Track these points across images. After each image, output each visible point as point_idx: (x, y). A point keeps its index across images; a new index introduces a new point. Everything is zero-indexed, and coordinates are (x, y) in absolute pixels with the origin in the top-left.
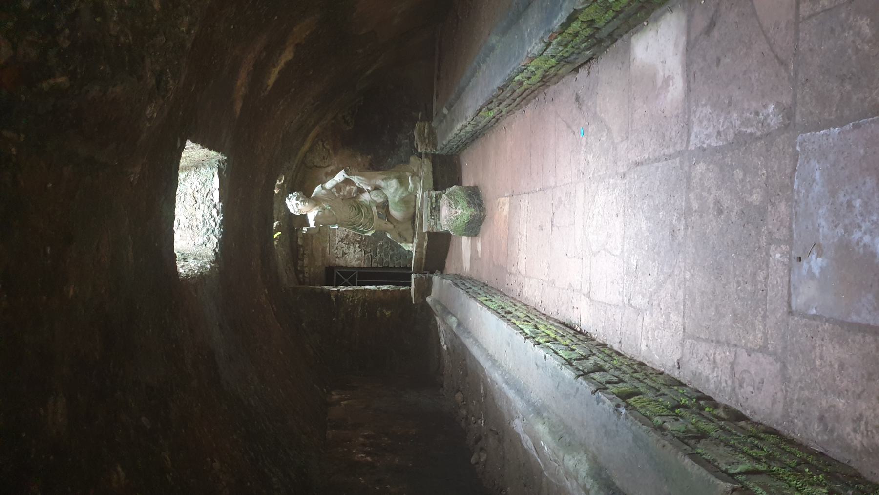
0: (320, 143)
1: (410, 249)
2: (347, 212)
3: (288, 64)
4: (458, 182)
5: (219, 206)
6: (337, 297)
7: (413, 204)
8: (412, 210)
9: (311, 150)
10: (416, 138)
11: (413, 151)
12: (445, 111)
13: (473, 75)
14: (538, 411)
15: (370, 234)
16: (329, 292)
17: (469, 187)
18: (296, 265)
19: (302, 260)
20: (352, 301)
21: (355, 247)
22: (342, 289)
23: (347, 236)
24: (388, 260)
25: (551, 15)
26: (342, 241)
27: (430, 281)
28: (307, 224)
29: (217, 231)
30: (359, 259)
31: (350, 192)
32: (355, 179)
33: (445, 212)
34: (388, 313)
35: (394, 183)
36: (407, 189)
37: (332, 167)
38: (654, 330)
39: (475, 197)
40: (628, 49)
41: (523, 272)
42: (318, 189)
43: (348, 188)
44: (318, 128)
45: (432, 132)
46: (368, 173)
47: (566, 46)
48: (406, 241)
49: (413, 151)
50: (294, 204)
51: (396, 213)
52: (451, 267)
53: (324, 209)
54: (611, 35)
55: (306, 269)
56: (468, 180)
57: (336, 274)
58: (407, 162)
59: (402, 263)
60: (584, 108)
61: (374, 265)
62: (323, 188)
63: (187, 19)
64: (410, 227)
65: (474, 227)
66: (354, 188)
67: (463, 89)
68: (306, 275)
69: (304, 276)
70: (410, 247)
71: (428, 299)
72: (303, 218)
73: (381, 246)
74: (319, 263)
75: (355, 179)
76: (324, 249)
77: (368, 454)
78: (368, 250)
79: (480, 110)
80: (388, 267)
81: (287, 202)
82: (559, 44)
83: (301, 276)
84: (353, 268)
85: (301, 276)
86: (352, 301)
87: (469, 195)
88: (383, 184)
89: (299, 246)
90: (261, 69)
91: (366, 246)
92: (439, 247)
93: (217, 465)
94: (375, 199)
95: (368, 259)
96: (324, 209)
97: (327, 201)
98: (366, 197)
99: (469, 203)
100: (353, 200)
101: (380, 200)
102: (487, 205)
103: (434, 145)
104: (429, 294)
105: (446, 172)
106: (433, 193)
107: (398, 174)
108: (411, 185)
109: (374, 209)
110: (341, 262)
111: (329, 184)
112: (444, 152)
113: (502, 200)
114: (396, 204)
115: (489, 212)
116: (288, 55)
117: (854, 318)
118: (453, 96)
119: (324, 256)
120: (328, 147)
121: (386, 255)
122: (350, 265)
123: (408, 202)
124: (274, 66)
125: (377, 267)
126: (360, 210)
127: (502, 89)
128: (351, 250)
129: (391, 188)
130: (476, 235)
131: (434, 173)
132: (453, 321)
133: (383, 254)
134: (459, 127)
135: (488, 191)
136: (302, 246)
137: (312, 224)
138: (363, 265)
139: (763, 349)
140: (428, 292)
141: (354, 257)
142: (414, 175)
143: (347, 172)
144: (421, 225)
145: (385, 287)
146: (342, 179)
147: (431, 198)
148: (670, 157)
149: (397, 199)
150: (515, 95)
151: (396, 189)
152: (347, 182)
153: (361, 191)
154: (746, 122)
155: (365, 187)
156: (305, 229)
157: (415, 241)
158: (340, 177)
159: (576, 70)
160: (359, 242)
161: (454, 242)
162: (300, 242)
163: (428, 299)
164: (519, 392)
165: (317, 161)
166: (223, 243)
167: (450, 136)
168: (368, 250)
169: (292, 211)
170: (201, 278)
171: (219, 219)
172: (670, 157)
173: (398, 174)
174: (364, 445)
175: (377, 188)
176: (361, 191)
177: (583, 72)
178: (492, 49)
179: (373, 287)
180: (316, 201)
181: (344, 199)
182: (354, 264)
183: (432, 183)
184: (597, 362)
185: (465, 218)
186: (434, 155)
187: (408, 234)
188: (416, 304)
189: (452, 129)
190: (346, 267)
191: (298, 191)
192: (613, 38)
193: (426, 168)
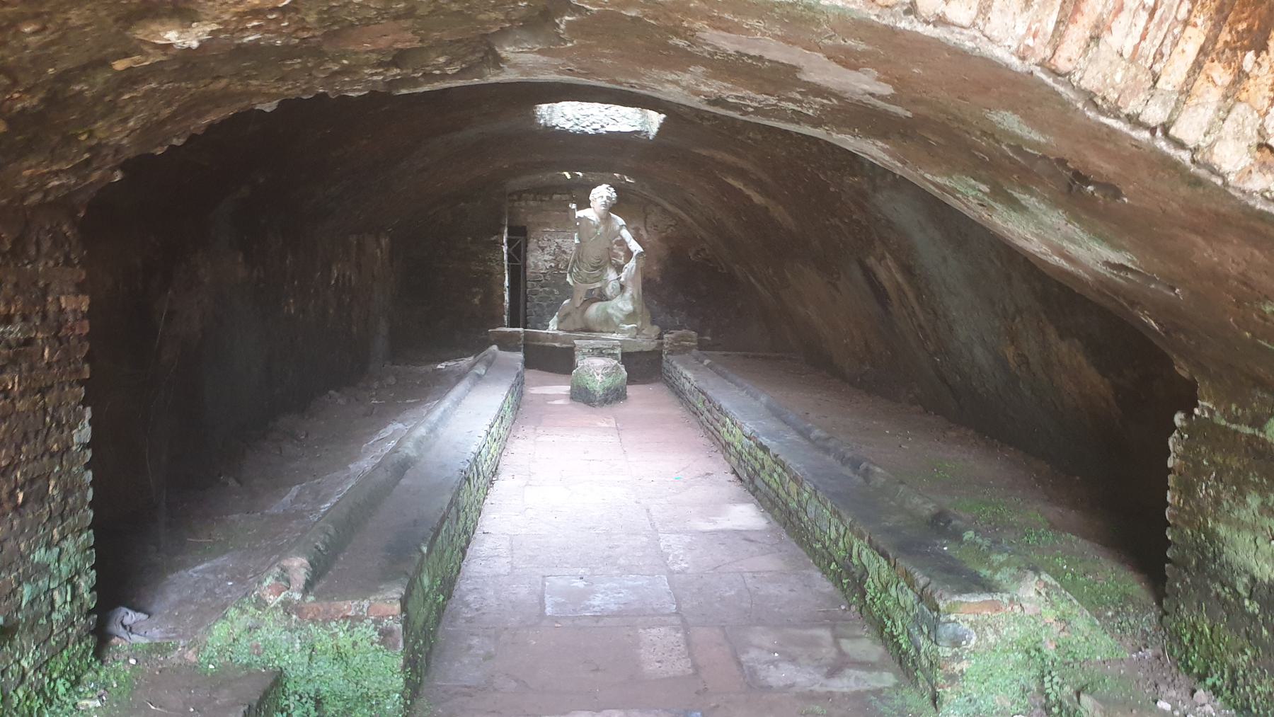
1: (551, 327)
2: (593, 253)
3: (748, 197)
4: (631, 380)
5: (602, 131)
6: (496, 242)
8: (598, 328)
9: (664, 210)
10: (679, 332)
11: (664, 329)
12: (707, 362)
13: (737, 385)
14: (432, 430)
15: (569, 279)
16: (502, 234)
17: (625, 390)
18: (528, 191)
19: (535, 199)
20: (490, 260)
22: (505, 249)
23: (564, 252)
24: (536, 302)
25: (768, 434)
26: (559, 247)
27: (517, 349)
28: (579, 208)
29: (576, 128)
30: (536, 266)
31: (616, 256)
32: (632, 264)
33: (599, 362)
34: (476, 301)
35: (629, 307)
36: (622, 322)
37: (645, 236)
39: (615, 396)
40: (743, 501)
41: (539, 439)
42: (621, 221)
43: (622, 253)
44: (689, 220)
45: (686, 349)
46: (639, 279)
47: (750, 454)
48: (560, 322)
49: (664, 329)
50: (602, 194)
51: (594, 310)
52: (530, 375)
53: (597, 227)
54: (756, 488)
55: (523, 204)
56: (632, 391)
57: (520, 236)
58: (653, 323)
59: (531, 318)
63: (759, 137)
64: (578, 327)
65: (582, 395)
66: (621, 261)
67: (725, 378)
68: (516, 204)
70: (553, 326)
71: (495, 347)
72: (585, 204)
73: (552, 292)
75: (632, 264)
77: (337, 280)
78: (548, 277)
79: (704, 393)
80: (527, 301)
81: (605, 186)
82: (750, 447)
83: (515, 197)
84: (526, 259)
85: (515, 197)
86: (490, 260)
87: (617, 390)
88: (627, 295)
90: (741, 174)
91: (552, 275)
92: (555, 360)
93: (365, 142)
96: (597, 227)
97: (606, 230)
98: (612, 275)
99: (608, 389)
100: (611, 258)
101: (609, 291)
102: (606, 408)
103: (671, 353)
104: (500, 349)
105: (643, 367)
106: (618, 351)
107: (638, 311)
108: (627, 327)
109: (598, 285)
111: (626, 234)
112: (665, 364)
113: (613, 421)
114: (605, 310)
115: (599, 409)
116: (757, 199)
117: (547, 596)
118: (720, 368)
121: (542, 299)
123: (608, 323)
124: (745, 185)
126: (597, 268)
127: (720, 409)
128: (547, 257)
129: (623, 305)
130: (572, 398)
131: (641, 352)
132: (481, 370)
134: (689, 375)
135: (621, 409)
138: (529, 271)
139: (513, 568)
140: (503, 347)
141: (539, 260)
142: (639, 331)
143: (640, 254)
144: (580, 338)
145: (507, 298)
146: (632, 248)
147: (613, 349)
148: (653, 525)
149: (610, 311)
150: (715, 423)
152: (629, 254)
153: (619, 269)
154: (676, 556)
155: (623, 275)
156: (574, 206)
157: (561, 333)
158: (635, 247)
159: (734, 472)
161: (563, 378)
162: (556, 197)
163: (495, 347)
164: (441, 419)
165: (652, 218)
166: (564, 133)
167: (680, 368)
169: (594, 191)
170: (533, 118)
171: (590, 130)
172: (653, 525)
173: (638, 311)
174: (344, 276)
175: (622, 287)
176: (619, 269)
177: (733, 477)
178: (756, 398)
179: (506, 283)
180: (606, 219)
181: (610, 249)
182: (531, 260)
184: (475, 479)
185: (591, 385)
186: (660, 353)
187: (568, 323)
188: (487, 333)
189: (687, 368)
190: (526, 251)
192: (755, 491)
193: (646, 343)
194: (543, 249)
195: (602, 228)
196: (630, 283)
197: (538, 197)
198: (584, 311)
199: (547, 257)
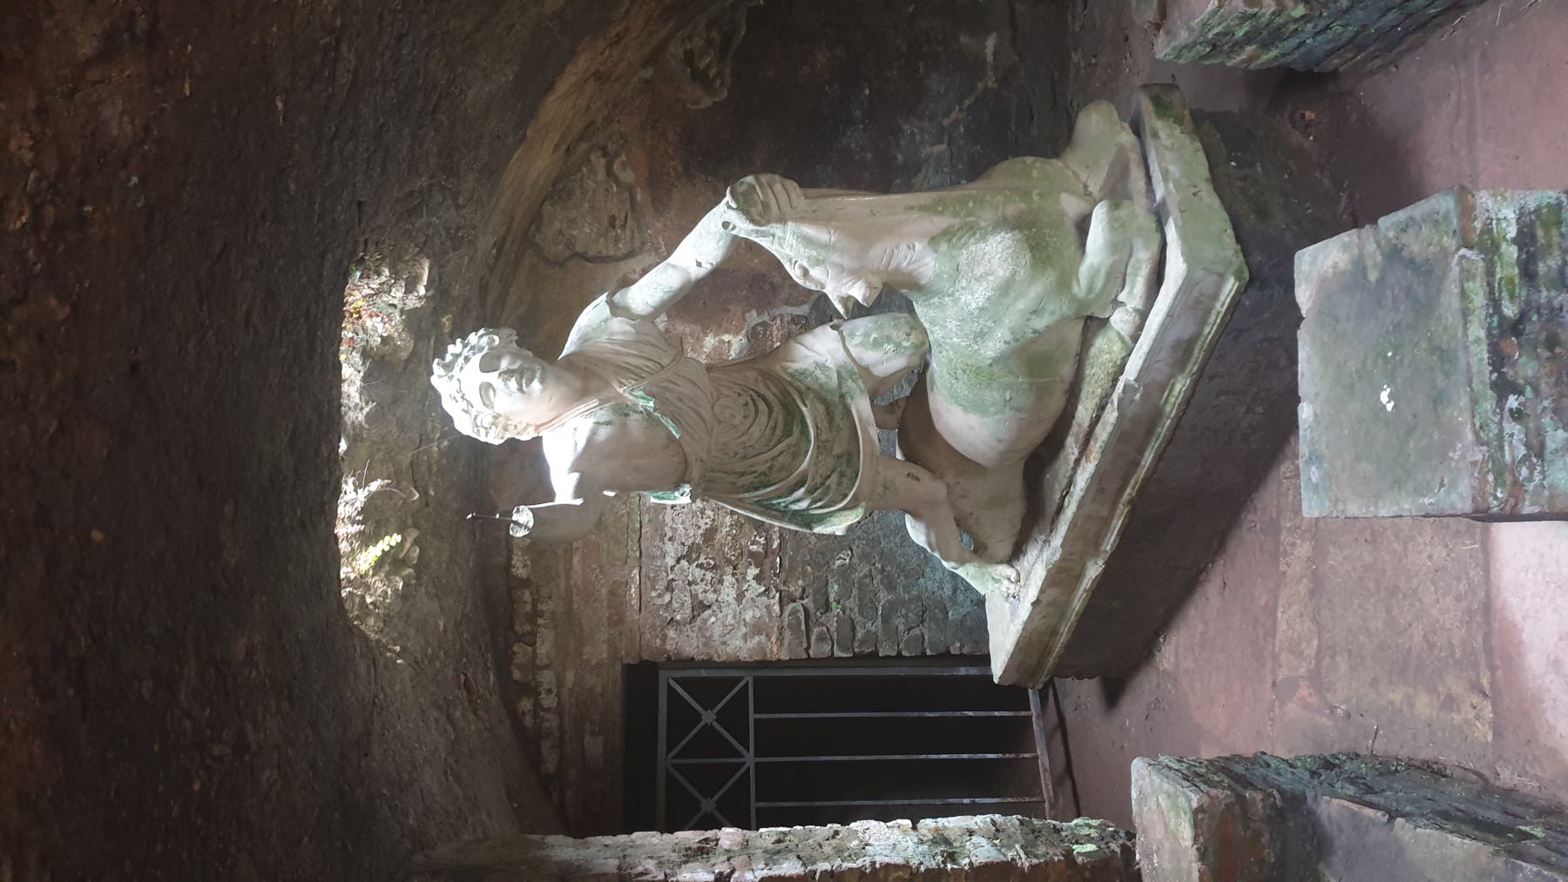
0: (599, 162)
7: (1067, 371)
8: (1056, 402)
18: (503, 662)
21: (741, 580)
23: (709, 534)
24: (876, 626)
26: (690, 554)
30: (757, 628)
35: (995, 254)
36: (1064, 283)
38: (919, 598)
42: (593, 317)
50: (479, 394)
55: (547, 678)
60: (1487, 76)
61: (819, 650)
62: (616, 309)
68: (548, 701)
69: (537, 706)
72: (523, 457)
73: (845, 572)
74: (597, 651)
76: (617, 593)
78: (795, 588)
83: (526, 704)
84: (737, 664)
85: (526, 704)
88: (926, 263)
89: (515, 584)
91: (789, 573)
94: (869, 357)
95: (794, 628)
97: (634, 373)
101: (887, 360)
109: (862, 407)
110: (686, 643)
111: (648, 291)
114: (982, 375)
119: (618, 620)
120: (628, 176)
121: (868, 606)
122: (722, 653)
125: (831, 660)
126: (792, 416)
128: (728, 592)
133: (852, 603)
136: (525, 583)
137: (564, 488)
138: (778, 651)
141: (737, 621)
149: (992, 348)
151: (1005, 289)
158: (701, 248)
160: (757, 559)
162: (520, 569)
165: (585, 234)
168: (795, 588)
169: (464, 426)
180: (585, 376)
183: (1229, 236)
190: (708, 663)
191: (490, 322)
194: (700, 607)
195: (627, 392)
196: (878, 254)
197: (522, 627)
198: (962, 464)
199: (728, 592)
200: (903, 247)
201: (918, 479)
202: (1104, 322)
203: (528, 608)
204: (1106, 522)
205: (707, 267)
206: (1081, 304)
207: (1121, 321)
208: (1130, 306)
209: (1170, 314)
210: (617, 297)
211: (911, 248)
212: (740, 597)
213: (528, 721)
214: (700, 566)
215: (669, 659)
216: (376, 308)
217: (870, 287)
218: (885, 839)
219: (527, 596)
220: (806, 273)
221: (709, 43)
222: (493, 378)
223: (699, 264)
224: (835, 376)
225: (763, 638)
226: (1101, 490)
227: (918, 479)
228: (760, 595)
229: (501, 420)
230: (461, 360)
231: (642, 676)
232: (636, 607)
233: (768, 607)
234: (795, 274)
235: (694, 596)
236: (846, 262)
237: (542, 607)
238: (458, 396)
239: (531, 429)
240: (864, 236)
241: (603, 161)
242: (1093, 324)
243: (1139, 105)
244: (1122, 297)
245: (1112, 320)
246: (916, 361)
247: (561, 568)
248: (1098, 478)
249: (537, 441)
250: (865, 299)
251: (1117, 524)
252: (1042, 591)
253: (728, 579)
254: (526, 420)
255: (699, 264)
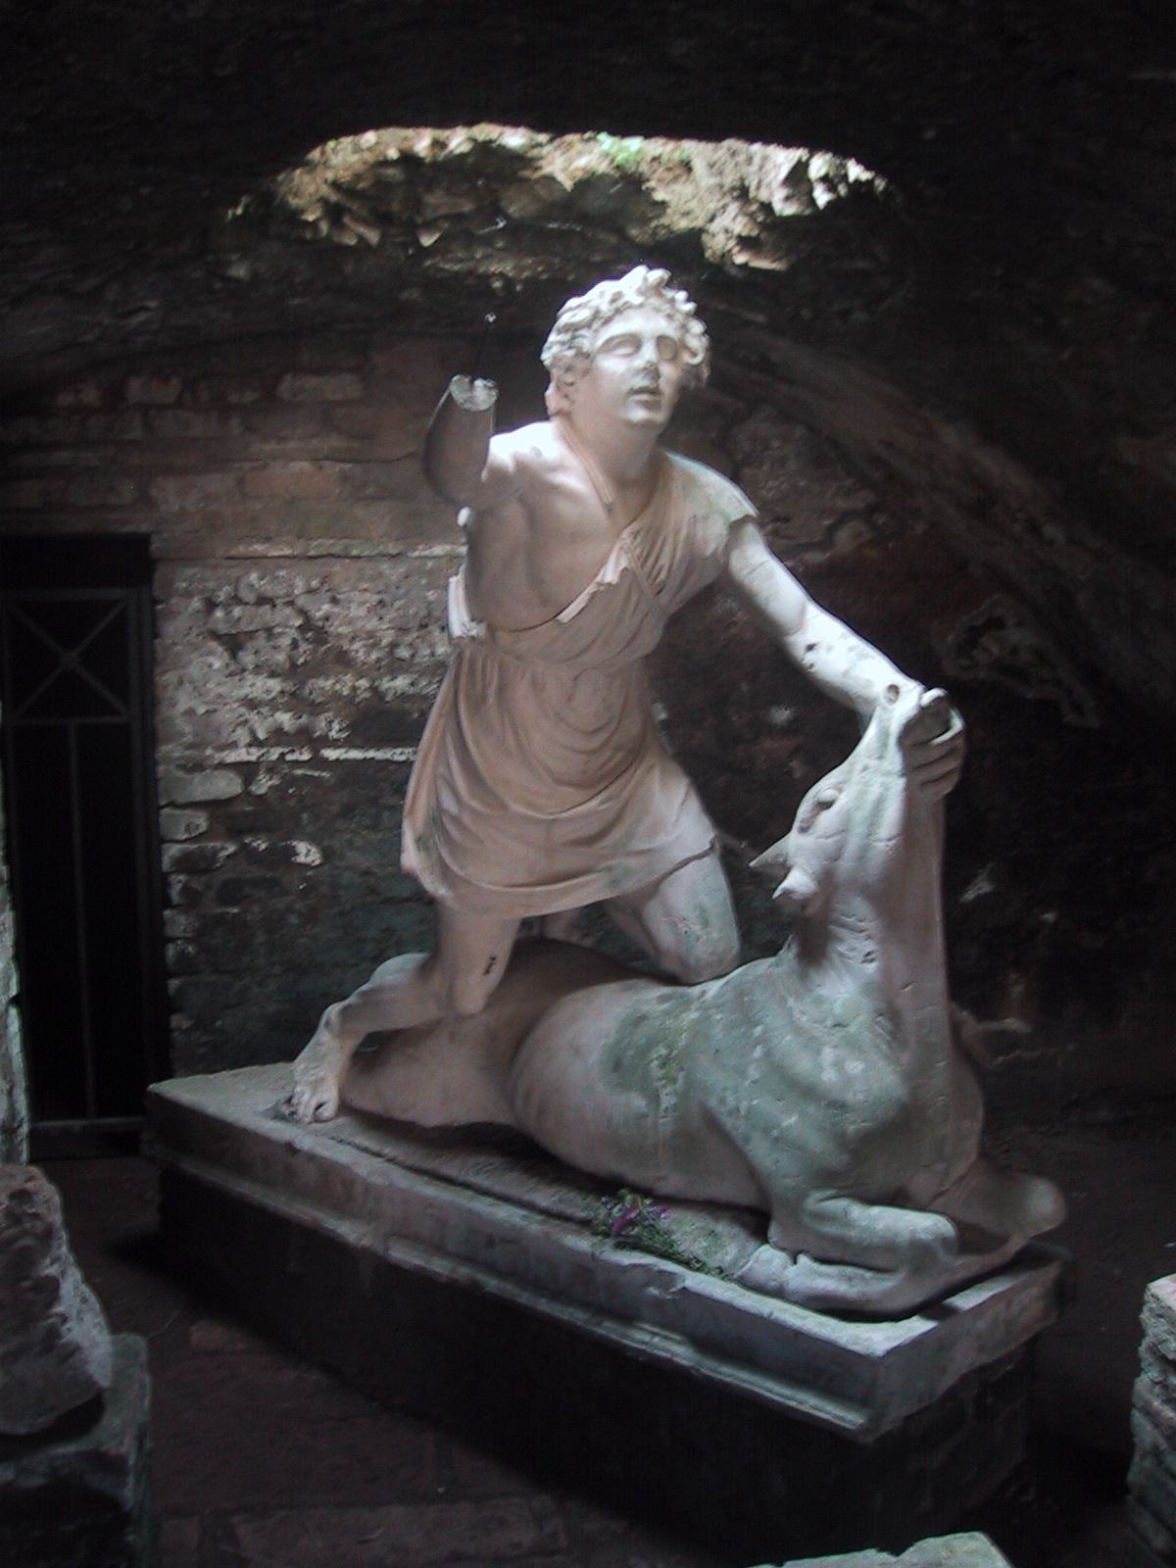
50: (628, 329)
62: (736, 527)
110: (180, 623)
151: (806, 1091)
194: (234, 644)
196: (858, 910)
200: (869, 946)
201: (487, 972)
202: (761, 1235)
203: (233, 398)
204: (438, 1249)
205: (809, 658)
206: (795, 1208)
207: (768, 1260)
208: (792, 1270)
209: (798, 1335)
210: (751, 530)
211: (868, 958)
212: (252, 704)
213: (66, 399)
214: (295, 645)
215: (156, 602)
216: (729, 185)
217: (805, 903)
218: (14, 1025)
219: (249, 397)
220: (826, 805)
221: (1015, 651)
222: (649, 353)
223: (810, 648)
224: (646, 846)
225: (189, 739)
226: (490, 1242)
227: (487, 972)
228: (253, 733)
229: (581, 364)
230: (666, 308)
231: (133, 564)
232: (233, 553)
233: (234, 745)
234: (824, 788)
235: (251, 635)
236: (846, 864)
237: (235, 422)
238: (620, 303)
239: (564, 404)
240: (887, 895)
241: (861, 506)
242: (756, 1221)
243: (494, 999)
244: (803, 1259)
245: (766, 1247)
246: (670, 965)
247: (292, 445)
248: (512, 1239)
249: (543, 415)
250: (787, 893)
251: (440, 1266)
252: (312, 1157)
253: (276, 685)
254: (580, 398)
255: (810, 648)
